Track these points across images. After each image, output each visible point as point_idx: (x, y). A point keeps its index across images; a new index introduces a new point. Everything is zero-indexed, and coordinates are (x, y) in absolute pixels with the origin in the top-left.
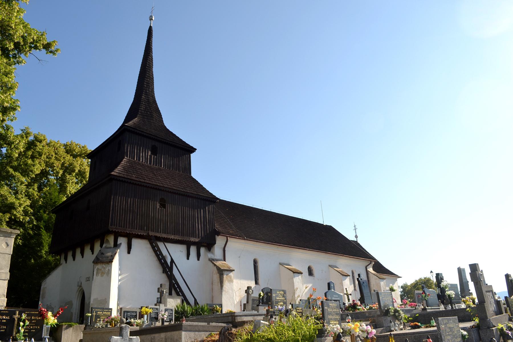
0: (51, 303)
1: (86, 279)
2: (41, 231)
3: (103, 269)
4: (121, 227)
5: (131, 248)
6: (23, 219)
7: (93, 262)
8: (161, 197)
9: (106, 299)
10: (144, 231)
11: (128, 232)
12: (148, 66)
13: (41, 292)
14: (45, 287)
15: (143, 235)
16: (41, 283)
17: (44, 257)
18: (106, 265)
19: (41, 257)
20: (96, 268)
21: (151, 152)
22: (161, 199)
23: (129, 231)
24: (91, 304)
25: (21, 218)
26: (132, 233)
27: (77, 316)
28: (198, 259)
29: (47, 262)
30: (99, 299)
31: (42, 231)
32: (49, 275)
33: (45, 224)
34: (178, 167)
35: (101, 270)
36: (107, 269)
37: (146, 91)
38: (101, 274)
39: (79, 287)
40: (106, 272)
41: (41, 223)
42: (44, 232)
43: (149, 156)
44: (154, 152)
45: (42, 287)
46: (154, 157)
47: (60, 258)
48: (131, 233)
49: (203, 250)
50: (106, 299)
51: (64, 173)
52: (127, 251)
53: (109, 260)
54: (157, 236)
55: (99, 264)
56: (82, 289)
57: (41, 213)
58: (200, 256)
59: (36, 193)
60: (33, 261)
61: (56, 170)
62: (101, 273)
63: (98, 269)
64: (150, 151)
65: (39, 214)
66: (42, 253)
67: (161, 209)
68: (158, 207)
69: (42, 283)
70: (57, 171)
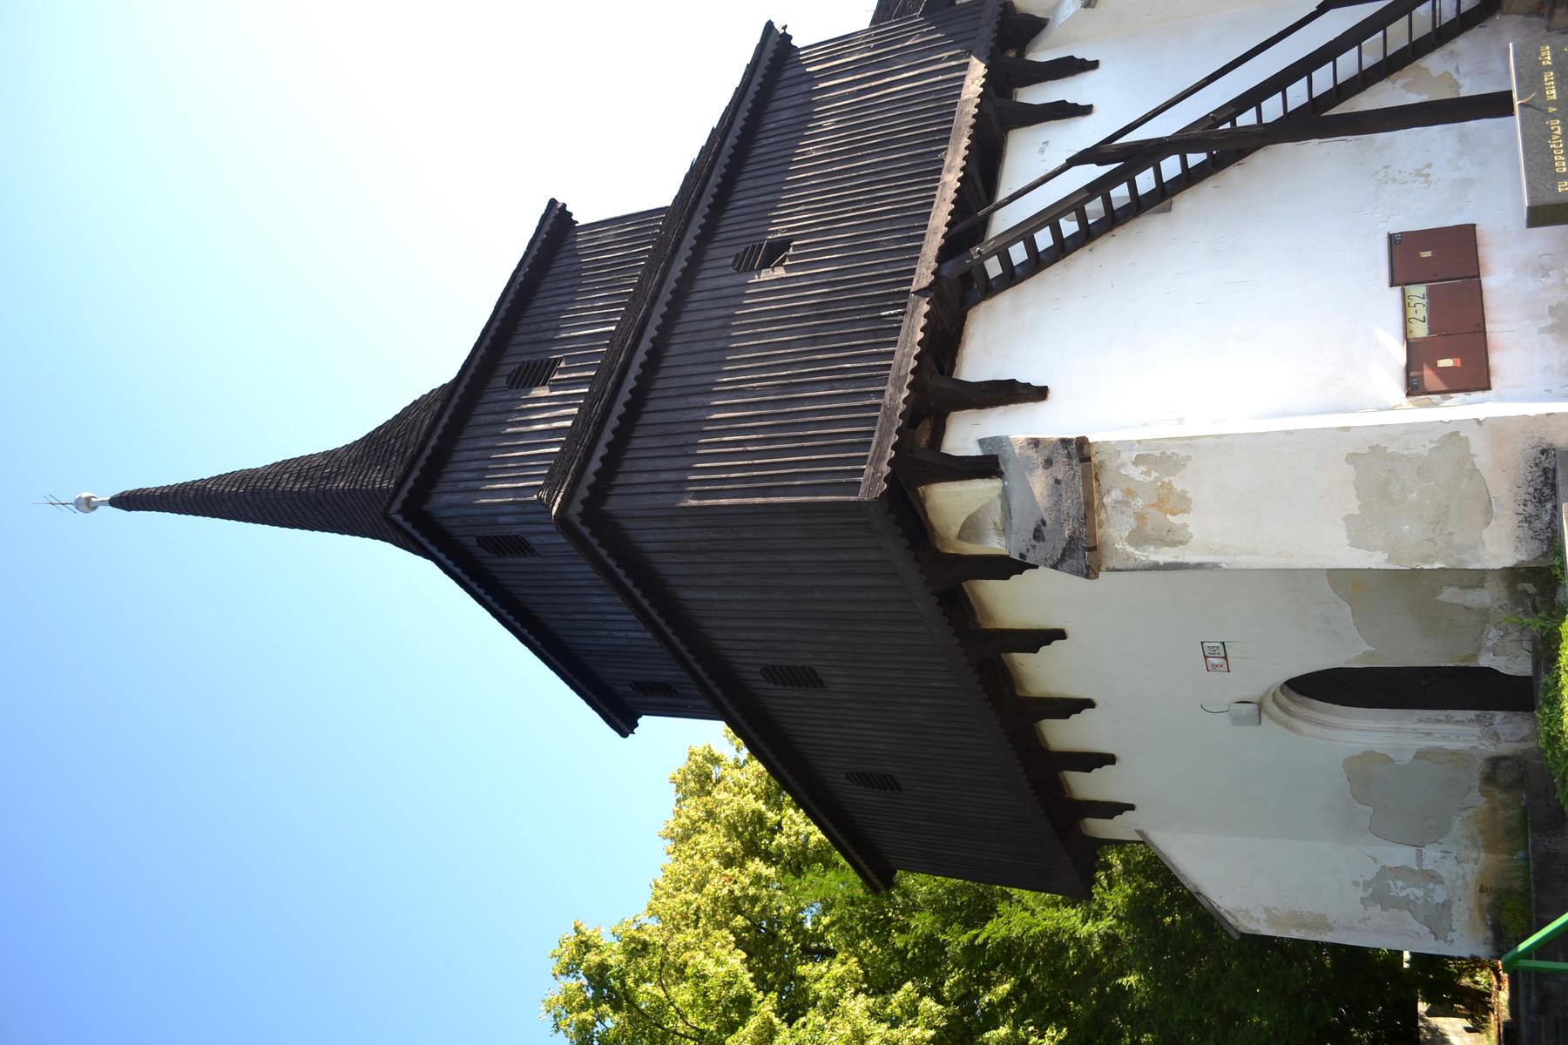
0: (1356, 883)
1: (1215, 666)
2: (985, 942)
3: (1139, 503)
4: (871, 433)
5: (1014, 381)
6: (929, 1026)
7: (1087, 576)
8: (731, 270)
9: (1351, 458)
10: (906, 319)
11: (906, 393)
12: (239, 488)
13: (1296, 934)
14: (1263, 917)
15: (926, 316)
16: (1243, 935)
17: (1110, 927)
18: (1105, 481)
19: (1110, 941)
20: (1130, 549)
21: (537, 385)
22: (738, 269)
23: (901, 391)
24: (1388, 561)
25: (919, 1036)
26: (913, 372)
27: (1438, 721)
28: (1094, 65)
29: (1140, 912)
30: (1354, 507)
31: (988, 938)
32: (1199, 894)
33: (955, 926)
34: (623, 263)
35: (1140, 518)
36: (1136, 473)
37: (324, 478)
38: (1175, 514)
39: (1264, 717)
40: (1154, 474)
41: (949, 943)
42: (993, 931)
43: (551, 391)
44: (539, 373)
45: (1266, 930)
46: (562, 371)
47: (1119, 844)
48: (910, 378)
49: (1042, 53)
50: (1351, 458)
51: (767, 857)
52: (1032, 404)
53: (1075, 462)
54: (941, 249)
55: (1099, 533)
56: (1275, 700)
57: (905, 946)
58: (1076, 104)
59: (838, 969)
60: (1131, 980)
61: (743, 889)
62: (1165, 513)
63: (1139, 537)
64: (530, 391)
65: (914, 954)
66: (1091, 935)
67: (792, 257)
68: (780, 272)
69: (1241, 929)
70: (751, 884)
